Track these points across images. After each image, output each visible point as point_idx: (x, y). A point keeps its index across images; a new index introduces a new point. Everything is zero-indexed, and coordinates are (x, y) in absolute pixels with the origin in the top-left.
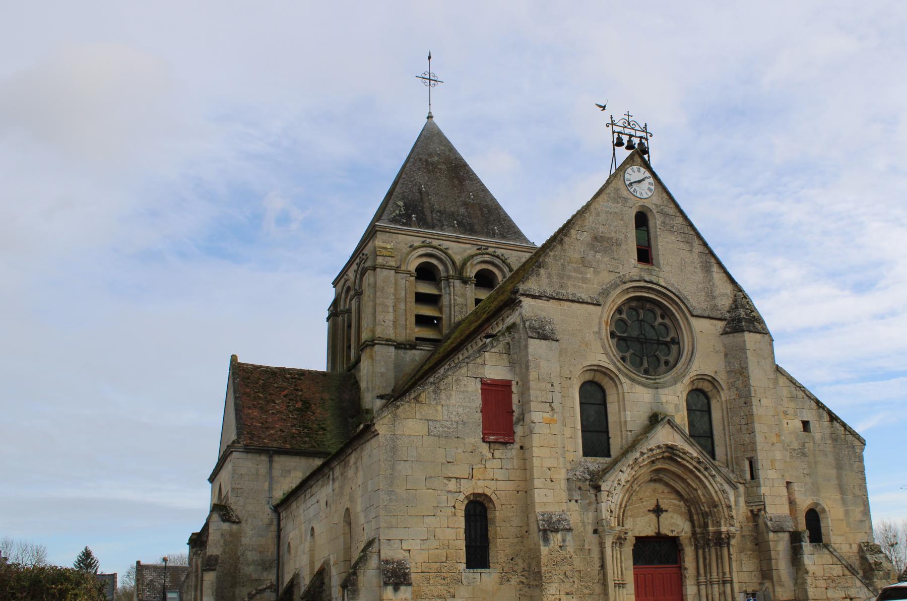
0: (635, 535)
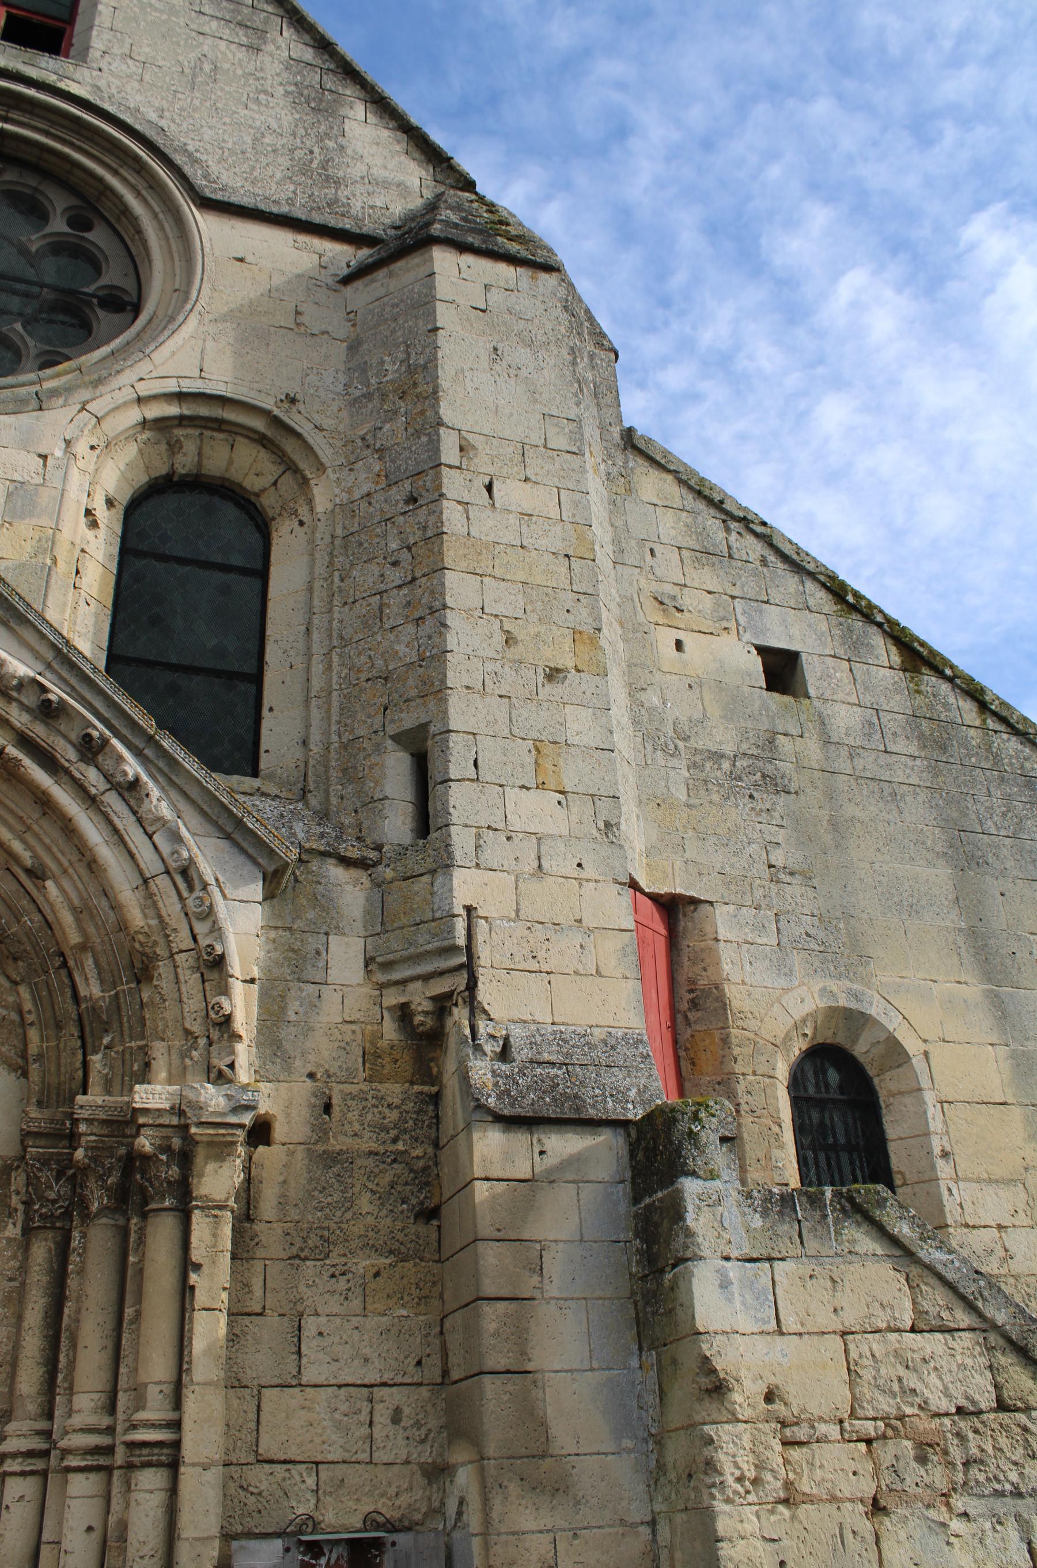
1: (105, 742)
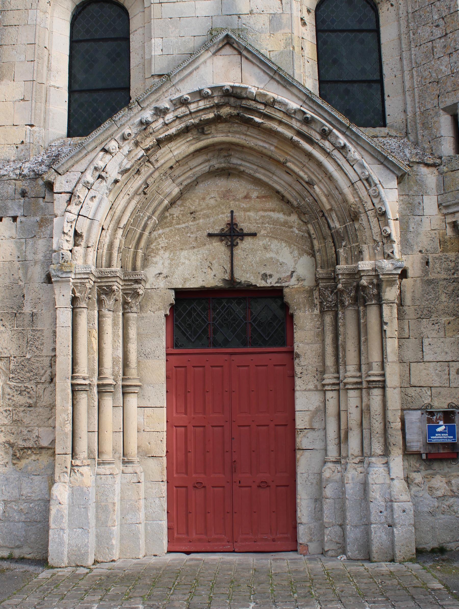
0: (174, 287)
1: (331, 131)
